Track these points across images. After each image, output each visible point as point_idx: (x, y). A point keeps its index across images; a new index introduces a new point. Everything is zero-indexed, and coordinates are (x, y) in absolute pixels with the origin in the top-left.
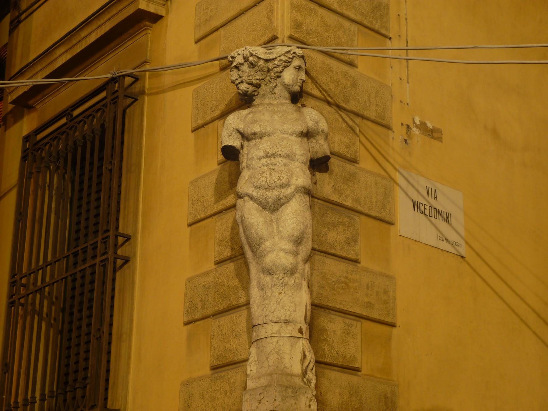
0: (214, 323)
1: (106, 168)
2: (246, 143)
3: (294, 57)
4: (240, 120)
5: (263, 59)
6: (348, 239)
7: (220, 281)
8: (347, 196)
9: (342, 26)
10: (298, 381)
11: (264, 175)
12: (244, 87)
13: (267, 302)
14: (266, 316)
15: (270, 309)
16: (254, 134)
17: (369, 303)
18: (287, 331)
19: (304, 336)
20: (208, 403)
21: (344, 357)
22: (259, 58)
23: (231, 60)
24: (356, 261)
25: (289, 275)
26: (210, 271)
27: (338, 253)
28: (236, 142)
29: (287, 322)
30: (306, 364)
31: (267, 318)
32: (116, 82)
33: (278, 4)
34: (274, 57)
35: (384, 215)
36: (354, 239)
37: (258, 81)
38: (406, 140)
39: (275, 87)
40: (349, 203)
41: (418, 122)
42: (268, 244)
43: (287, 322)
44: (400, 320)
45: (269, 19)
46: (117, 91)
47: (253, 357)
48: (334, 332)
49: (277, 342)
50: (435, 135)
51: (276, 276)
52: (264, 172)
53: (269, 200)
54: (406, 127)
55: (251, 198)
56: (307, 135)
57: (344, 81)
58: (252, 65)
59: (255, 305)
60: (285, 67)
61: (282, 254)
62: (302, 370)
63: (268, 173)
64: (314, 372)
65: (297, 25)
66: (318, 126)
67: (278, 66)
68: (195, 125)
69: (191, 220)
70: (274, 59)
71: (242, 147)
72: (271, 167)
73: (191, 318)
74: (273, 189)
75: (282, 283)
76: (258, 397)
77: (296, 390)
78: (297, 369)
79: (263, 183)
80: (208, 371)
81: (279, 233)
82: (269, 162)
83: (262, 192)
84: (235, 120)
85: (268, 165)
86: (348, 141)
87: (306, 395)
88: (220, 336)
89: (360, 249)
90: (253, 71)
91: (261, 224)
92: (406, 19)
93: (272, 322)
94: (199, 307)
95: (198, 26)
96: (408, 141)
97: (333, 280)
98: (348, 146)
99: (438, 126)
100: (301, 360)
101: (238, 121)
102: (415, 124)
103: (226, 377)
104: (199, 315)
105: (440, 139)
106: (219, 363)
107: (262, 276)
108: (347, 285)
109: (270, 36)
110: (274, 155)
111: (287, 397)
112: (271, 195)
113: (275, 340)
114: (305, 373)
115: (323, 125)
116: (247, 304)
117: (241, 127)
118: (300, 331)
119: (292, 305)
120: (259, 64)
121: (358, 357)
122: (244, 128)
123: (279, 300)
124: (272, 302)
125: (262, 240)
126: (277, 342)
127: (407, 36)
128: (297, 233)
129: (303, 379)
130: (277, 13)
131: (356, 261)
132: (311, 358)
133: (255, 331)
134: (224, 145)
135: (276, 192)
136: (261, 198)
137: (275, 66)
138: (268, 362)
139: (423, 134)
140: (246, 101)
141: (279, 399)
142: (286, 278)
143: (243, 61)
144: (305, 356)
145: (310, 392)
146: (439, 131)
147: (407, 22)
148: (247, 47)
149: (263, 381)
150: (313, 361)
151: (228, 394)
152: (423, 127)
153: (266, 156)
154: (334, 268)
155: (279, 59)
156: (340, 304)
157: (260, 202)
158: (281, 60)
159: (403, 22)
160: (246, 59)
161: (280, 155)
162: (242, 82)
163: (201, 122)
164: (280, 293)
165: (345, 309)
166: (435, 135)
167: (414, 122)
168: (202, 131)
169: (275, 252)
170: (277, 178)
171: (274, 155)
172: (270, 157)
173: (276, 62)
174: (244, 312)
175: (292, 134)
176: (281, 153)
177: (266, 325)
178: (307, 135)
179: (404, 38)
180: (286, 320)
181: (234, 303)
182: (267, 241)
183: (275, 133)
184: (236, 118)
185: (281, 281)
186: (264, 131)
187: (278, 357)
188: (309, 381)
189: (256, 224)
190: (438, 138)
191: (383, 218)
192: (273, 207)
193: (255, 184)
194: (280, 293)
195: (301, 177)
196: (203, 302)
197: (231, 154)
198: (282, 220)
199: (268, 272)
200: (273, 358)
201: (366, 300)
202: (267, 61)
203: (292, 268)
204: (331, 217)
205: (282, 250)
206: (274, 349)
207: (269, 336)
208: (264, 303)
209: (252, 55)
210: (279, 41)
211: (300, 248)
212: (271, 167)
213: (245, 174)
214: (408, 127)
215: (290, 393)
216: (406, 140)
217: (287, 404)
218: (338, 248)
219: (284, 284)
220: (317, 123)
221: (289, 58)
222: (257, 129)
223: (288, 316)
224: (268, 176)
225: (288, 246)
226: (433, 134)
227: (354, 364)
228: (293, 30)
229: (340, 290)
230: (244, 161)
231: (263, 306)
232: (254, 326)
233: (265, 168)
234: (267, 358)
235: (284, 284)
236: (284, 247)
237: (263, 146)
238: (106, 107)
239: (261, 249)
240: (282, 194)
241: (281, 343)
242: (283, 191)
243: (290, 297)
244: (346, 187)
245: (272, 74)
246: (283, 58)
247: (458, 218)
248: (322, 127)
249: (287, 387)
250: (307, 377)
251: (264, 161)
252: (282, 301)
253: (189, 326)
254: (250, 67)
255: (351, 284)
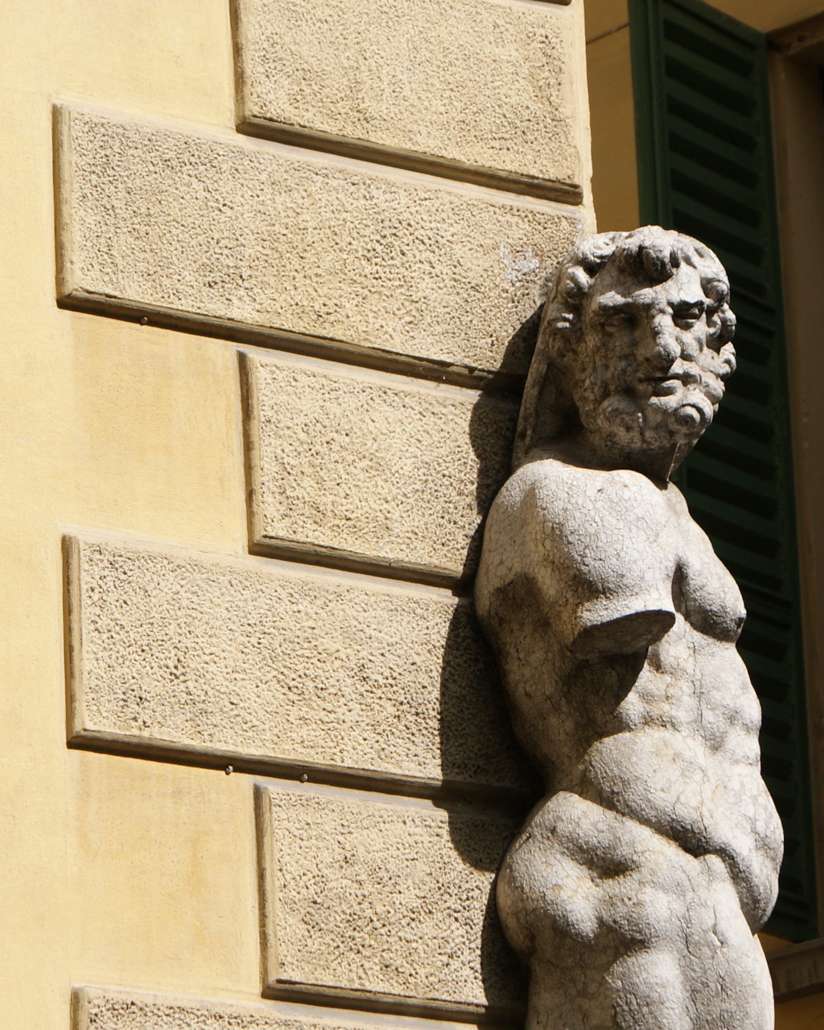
162: (687, 379)
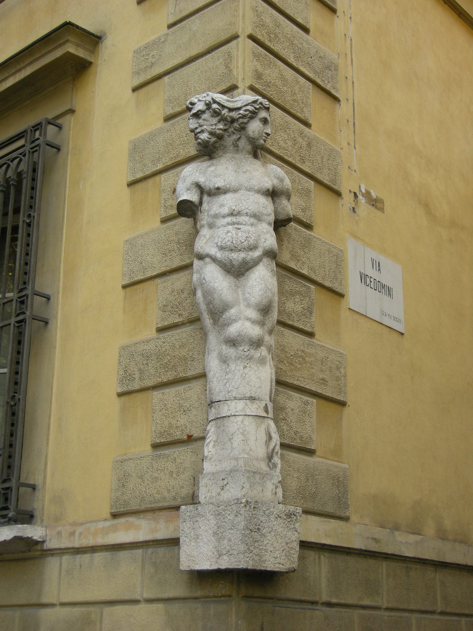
0: (157, 395)
1: (24, 221)
2: (205, 198)
3: (260, 107)
4: (200, 173)
5: (227, 108)
6: (304, 309)
7: (164, 349)
8: (304, 263)
9: (298, 82)
10: (264, 467)
11: (230, 234)
12: (204, 136)
13: (230, 376)
14: (229, 392)
15: (233, 384)
16: (218, 189)
17: (323, 379)
18: (253, 410)
19: (269, 416)
20: (148, 484)
21: (301, 438)
22: (223, 107)
23: (190, 106)
24: (311, 335)
25: (255, 347)
26: (153, 339)
27: (296, 324)
28: (192, 196)
29: (252, 399)
30: (271, 447)
31: (230, 394)
32: (38, 129)
33: (238, 51)
34: (239, 106)
35: (336, 286)
36: (309, 311)
37: (221, 132)
38: (353, 208)
39: (239, 139)
40: (305, 272)
41: (364, 191)
42: (233, 312)
43: (252, 399)
44: (350, 399)
45: (227, 67)
46: (38, 139)
47: (211, 437)
48: (292, 410)
49: (242, 421)
50: (379, 205)
51: (241, 348)
52: (228, 232)
53: (235, 263)
54: (353, 194)
55: (214, 260)
56: (273, 194)
57: (300, 140)
58: (216, 113)
59: (215, 379)
60: (252, 118)
61: (248, 324)
62: (268, 454)
63: (234, 232)
64: (279, 456)
65: (259, 76)
66: (283, 185)
67: (244, 116)
68: (131, 179)
69: (126, 282)
70: (239, 109)
71: (201, 203)
72: (237, 226)
73: (125, 389)
74: (240, 250)
75: (248, 356)
76: (222, 483)
77: (264, 476)
78: (261, 451)
79: (229, 243)
80: (148, 448)
81: (245, 300)
82: (234, 220)
83: (227, 253)
84: (192, 173)
85: (234, 224)
86: (304, 204)
87: (273, 481)
88: (164, 411)
89: (314, 323)
90: (215, 120)
91: (225, 289)
92: (353, 83)
93: (235, 398)
94: (137, 376)
95: (137, 73)
96: (355, 210)
97: (292, 354)
98: (304, 210)
99: (381, 197)
100: (266, 442)
101: (197, 174)
102: (362, 192)
103: (172, 457)
104: (136, 386)
105: (382, 210)
106: (162, 441)
107: (224, 347)
108: (304, 359)
109: (228, 85)
110: (239, 214)
111: (254, 483)
112: (237, 257)
113: (240, 419)
114: (270, 458)
115: (287, 183)
116: (203, 375)
117: (201, 180)
118: (266, 409)
119: (258, 380)
120: (223, 112)
121: (314, 437)
122: (204, 182)
123: (244, 375)
124: (236, 377)
125: (226, 307)
126: (242, 421)
127: (354, 100)
128: (265, 301)
129: (268, 465)
130: (237, 62)
131: (311, 335)
132: (277, 440)
133: (215, 408)
134: (181, 199)
135: (242, 255)
136: (225, 260)
137: (240, 115)
138: (232, 443)
139: (368, 203)
140: (208, 151)
141: (247, 486)
142: (252, 351)
143: (205, 107)
144: (270, 438)
145: (276, 478)
146: (382, 201)
147: (353, 86)
148: (210, 93)
149: (227, 465)
150: (278, 443)
151: (174, 475)
152: (367, 195)
153: (231, 214)
154: (294, 341)
155: (244, 108)
156: (298, 380)
157: (224, 264)
158: (246, 110)
159: (350, 83)
160: (208, 105)
161: (247, 213)
162: (202, 131)
163: (139, 175)
164: (245, 367)
165: (302, 385)
166: (379, 205)
167: (360, 191)
168: (139, 186)
169: (240, 322)
170: (245, 238)
171: (239, 214)
172: (236, 215)
173: (241, 112)
174: (196, 386)
175: (258, 191)
176: (248, 211)
177: (229, 402)
178: (273, 194)
179: (351, 102)
180: (252, 397)
181: (182, 375)
182: (232, 308)
183: (240, 189)
184: (195, 171)
185: (247, 353)
186: (228, 186)
187: (244, 438)
188: (275, 466)
189: (220, 288)
190: (381, 208)
191: (335, 289)
192: (238, 271)
193: (219, 244)
194: (245, 367)
195: (269, 239)
196: (141, 371)
197: (187, 210)
198: (249, 285)
199: (233, 342)
200: (237, 440)
201: (321, 376)
202: (231, 110)
203: (259, 340)
204: (293, 284)
205: (248, 319)
206: (238, 429)
207: (233, 414)
208: (226, 377)
209: (215, 102)
210: (240, 90)
211: (267, 318)
212: (237, 226)
213: (205, 232)
214: (355, 194)
215: (258, 480)
216: (353, 208)
217: (255, 491)
218: (296, 319)
219: (249, 357)
220: (282, 181)
221: (256, 108)
222: (220, 183)
223: (253, 393)
224: (234, 236)
225: (253, 314)
226: (376, 203)
227: (311, 446)
228: (254, 80)
229: (297, 365)
230: (204, 218)
231: (225, 381)
232: (212, 402)
233: (230, 227)
234: (230, 440)
235: (249, 357)
236: (250, 316)
237: (227, 202)
238: (24, 156)
239: (224, 316)
240: (249, 257)
241: (246, 423)
242: (250, 253)
243: (255, 371)
244: (302, 253)
245: (236, 125)
246: (249, 108)
247: (398, 292)
248: (286, 187)
249: (255, 473)
250: (273, 461)
251: (229, 219)
252: (247, 376)
253: (123, 398)
254: (212, 116)
255: (307, 359)
